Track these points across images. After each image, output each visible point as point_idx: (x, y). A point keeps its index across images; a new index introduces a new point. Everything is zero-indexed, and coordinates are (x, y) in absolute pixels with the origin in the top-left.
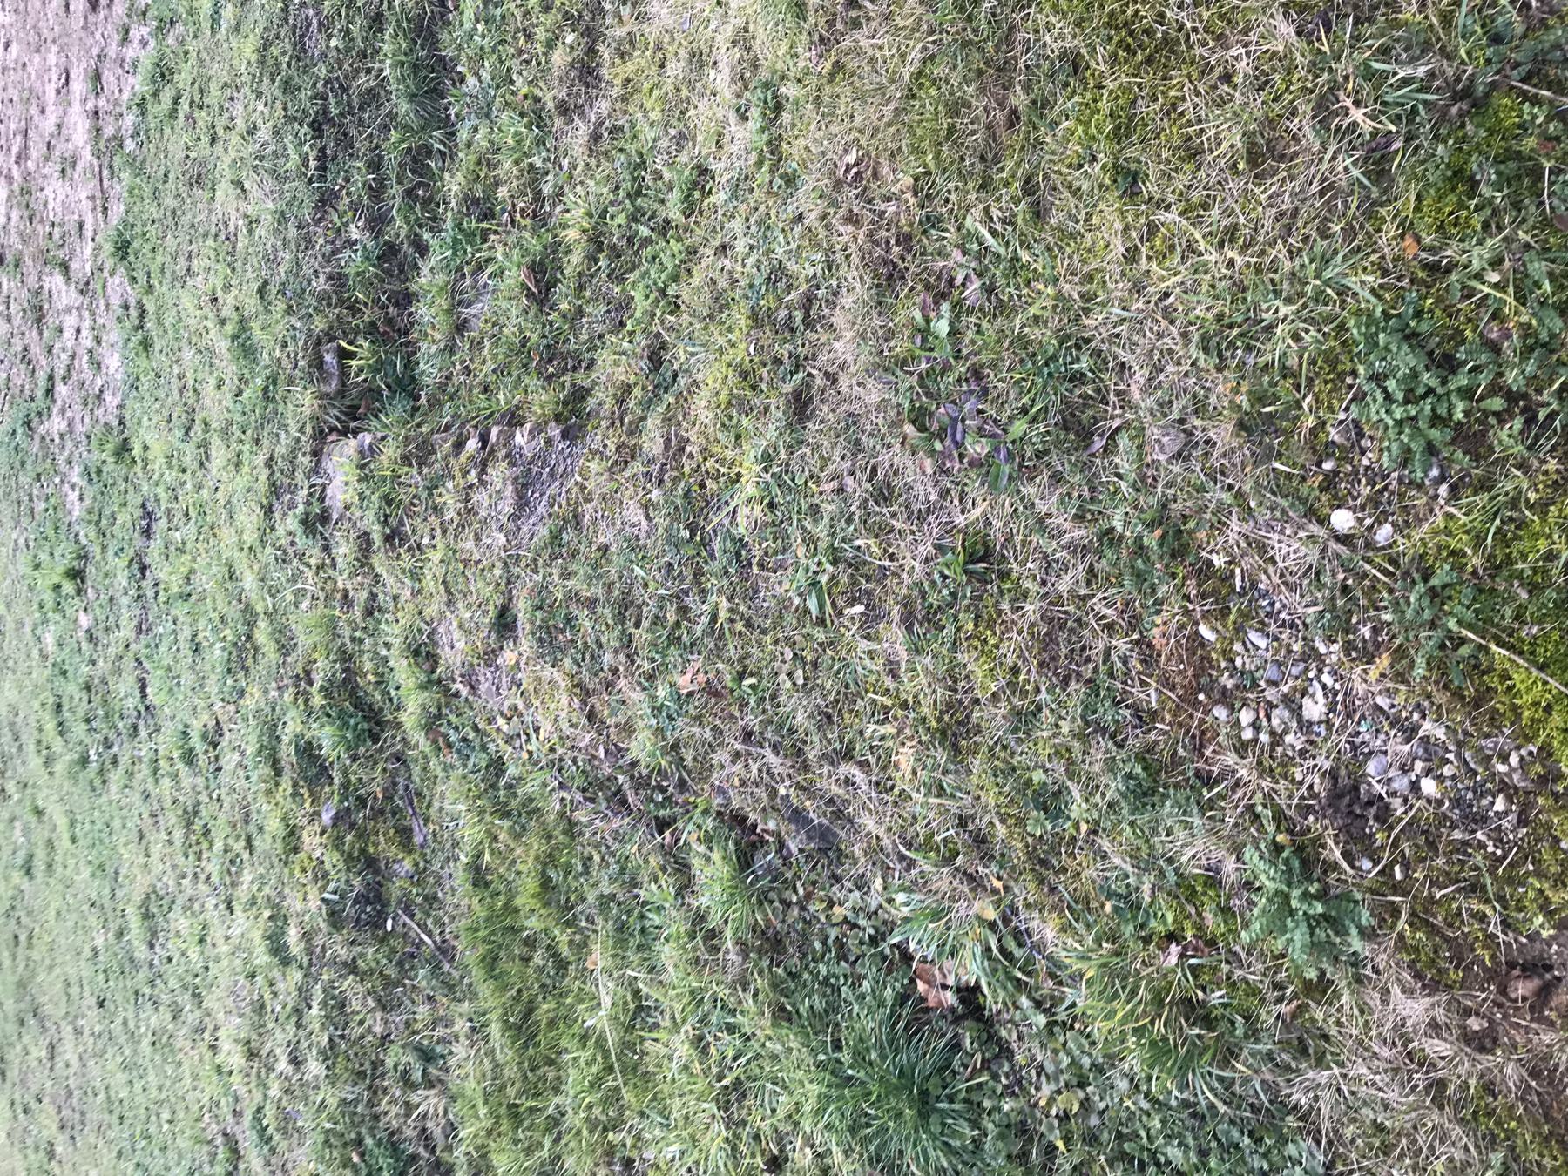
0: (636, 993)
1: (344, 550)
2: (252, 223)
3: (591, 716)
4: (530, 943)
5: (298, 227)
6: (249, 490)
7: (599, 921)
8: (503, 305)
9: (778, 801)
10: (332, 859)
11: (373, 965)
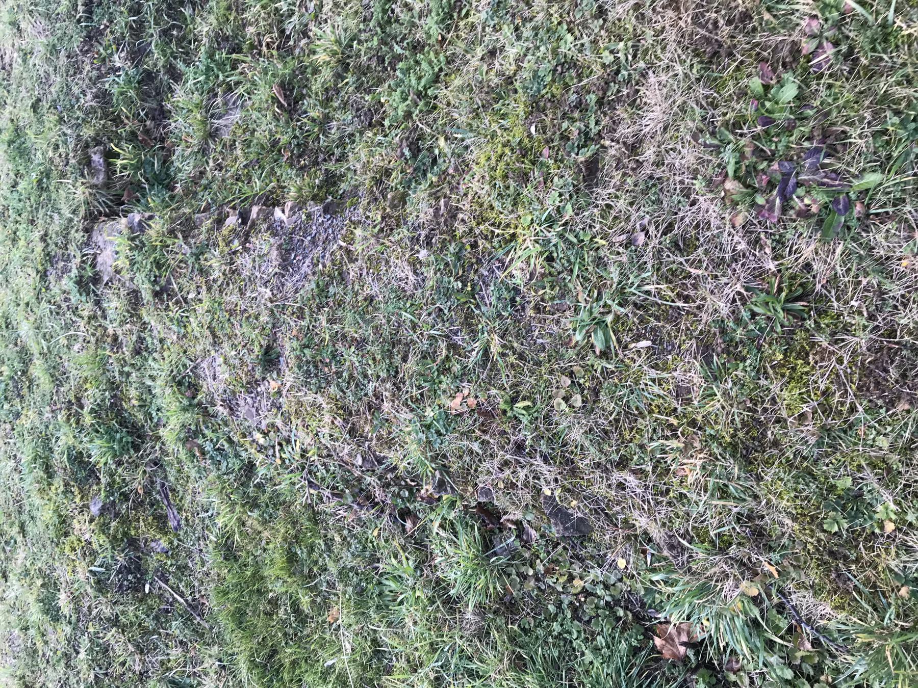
0: (375, 642)
1: (115, 304)
2: (26, 55)
3: (352, 432)
4: (275, 603)
5: (68, 57)
6: (25, 259)
7: (340, 587)
8: (254, 112)
9: (542, 500)
10: (99, 541)
11: (134, 619)
